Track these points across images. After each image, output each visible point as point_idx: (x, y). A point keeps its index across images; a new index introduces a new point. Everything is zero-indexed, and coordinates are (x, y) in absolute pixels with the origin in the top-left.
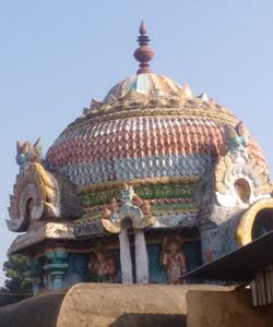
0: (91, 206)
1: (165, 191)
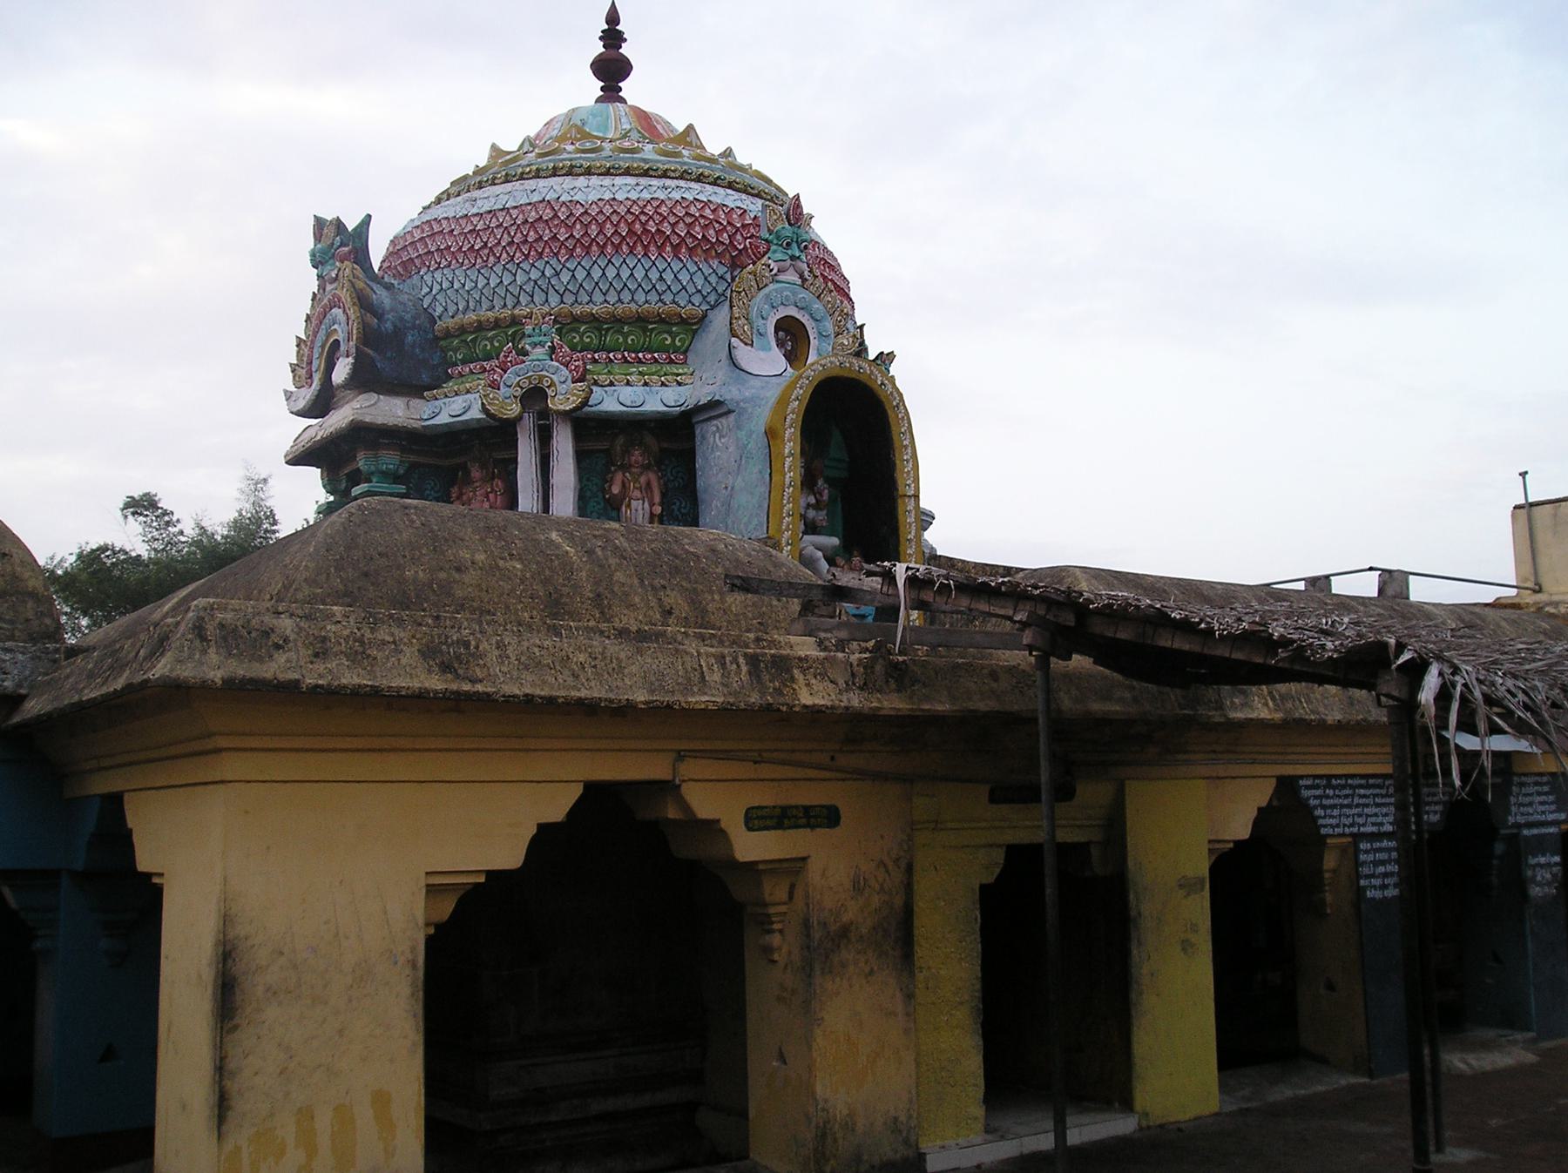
0: (464, 362)
1: (625, 336)
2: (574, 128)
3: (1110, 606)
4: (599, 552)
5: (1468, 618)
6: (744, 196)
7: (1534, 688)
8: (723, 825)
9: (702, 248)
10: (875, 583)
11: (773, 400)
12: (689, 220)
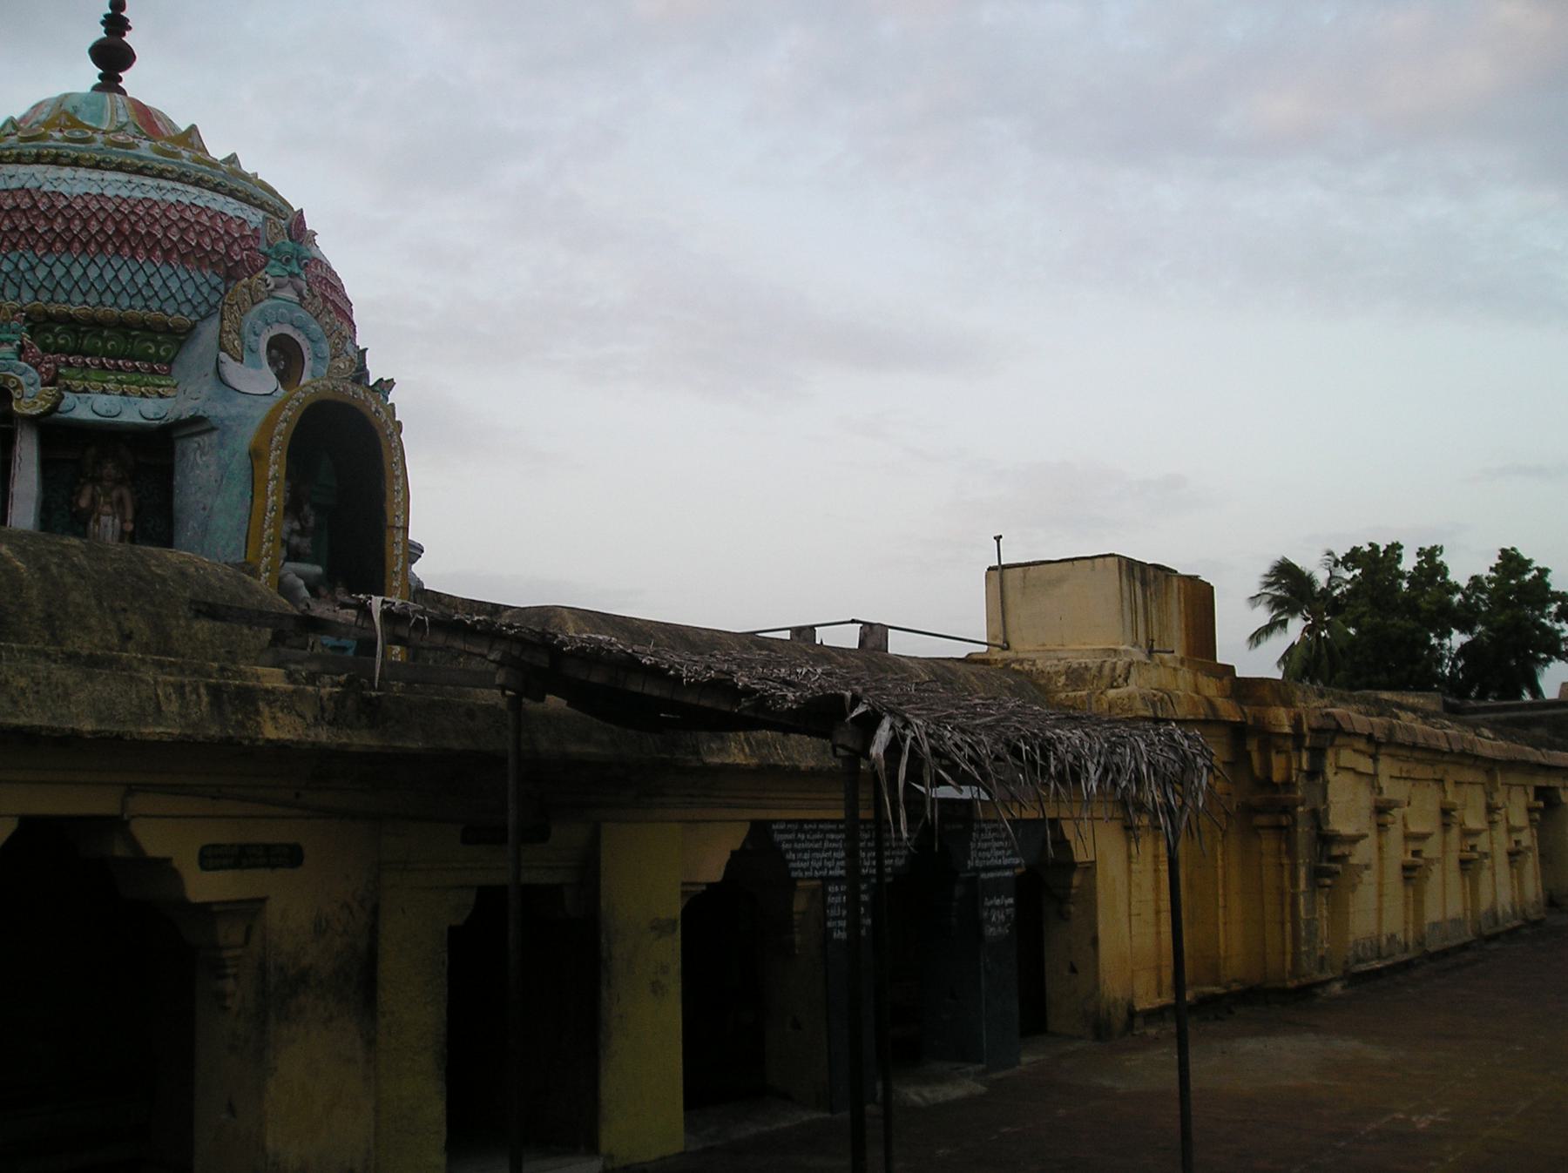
1: (56, 336)
2: (63, 114)
4: (54, 569)
6: (245, 206)
7: (980, 742)
8: (176, 864)
9: (195, 256)
10: (350, 615)
11: (257, 423)
12: (183, 225)
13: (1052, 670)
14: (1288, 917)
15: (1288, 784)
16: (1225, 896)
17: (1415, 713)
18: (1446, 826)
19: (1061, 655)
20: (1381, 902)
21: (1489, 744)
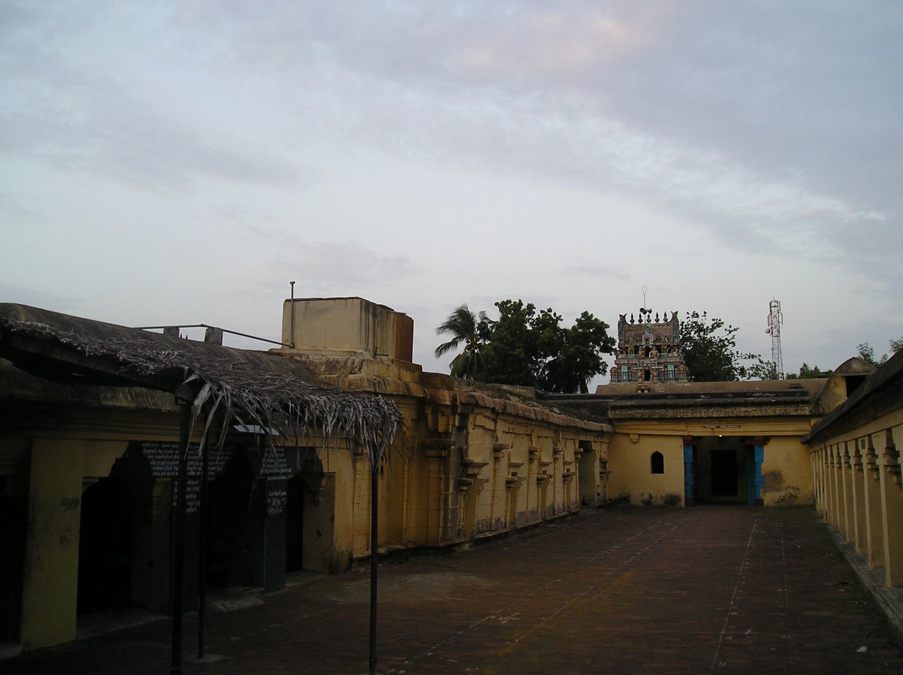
3: (24, 331)
5: (252, 357)
13: (318, 361)
14: (442, 507)
15: (447, 433)
16: (408, 494)
17: (519, 399)
18: (531, 460)
19: (324, 353)
20: (493, 500)
21: (557, 417)
